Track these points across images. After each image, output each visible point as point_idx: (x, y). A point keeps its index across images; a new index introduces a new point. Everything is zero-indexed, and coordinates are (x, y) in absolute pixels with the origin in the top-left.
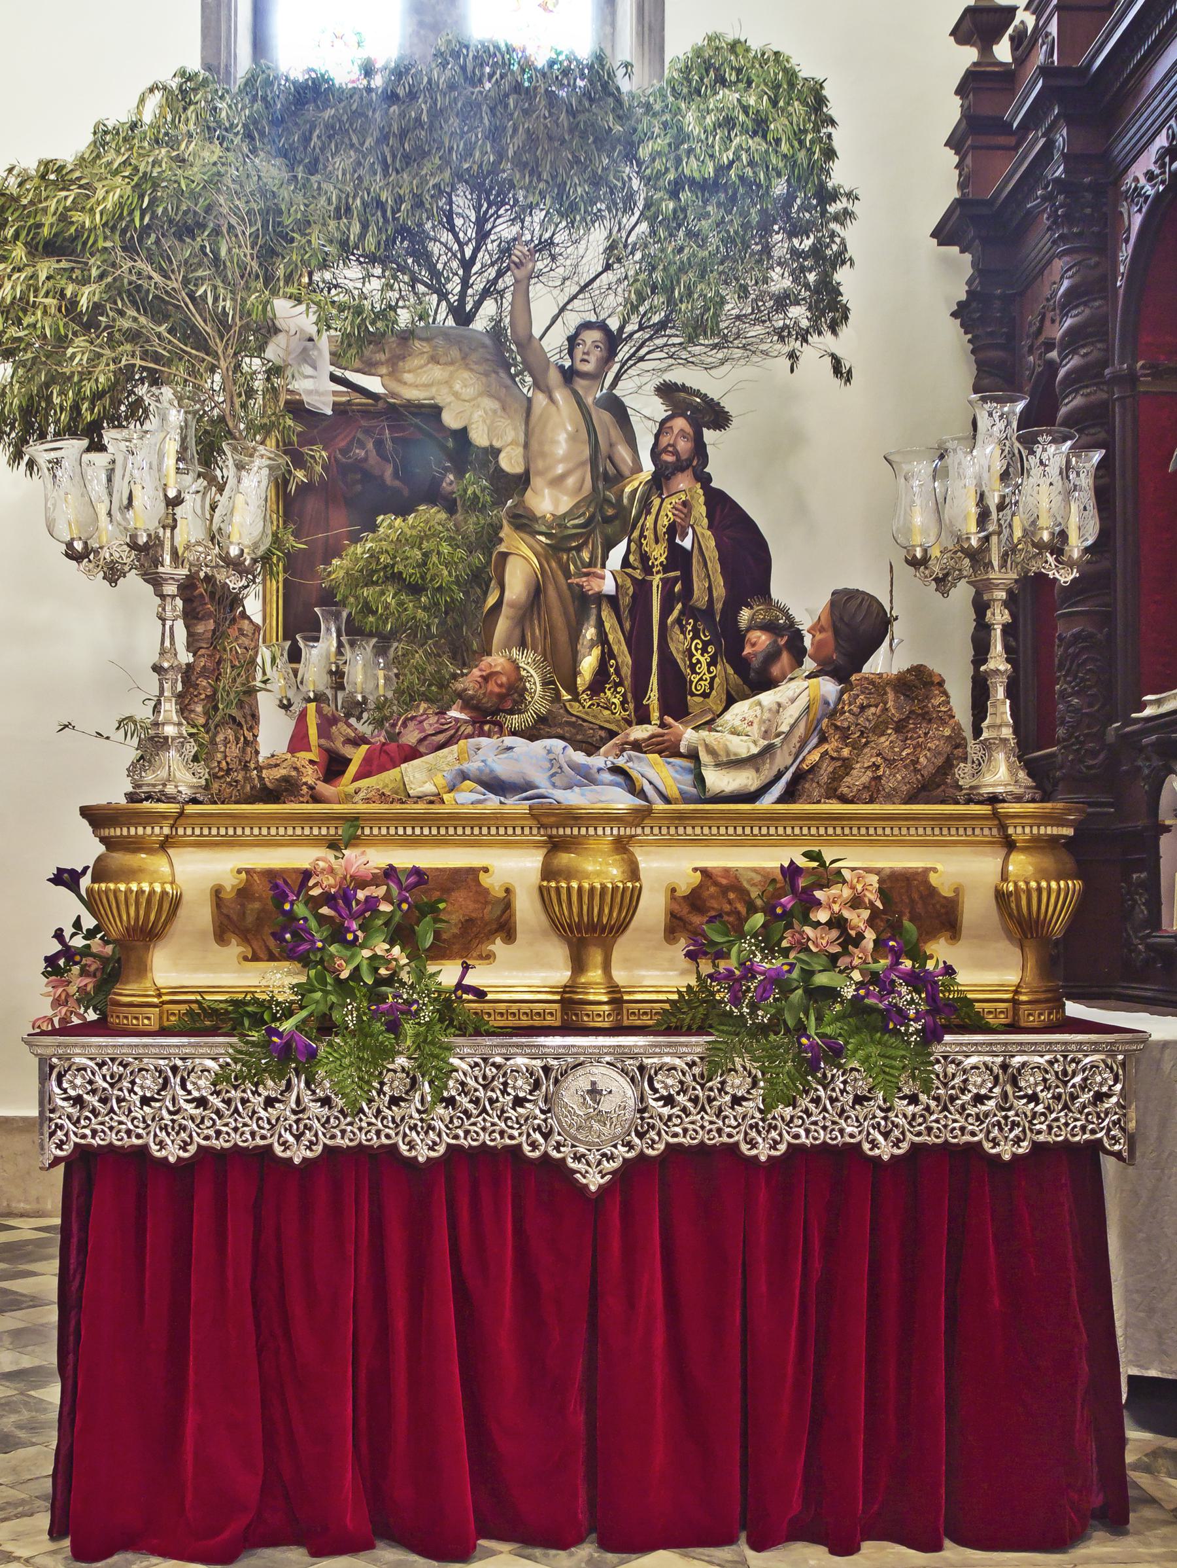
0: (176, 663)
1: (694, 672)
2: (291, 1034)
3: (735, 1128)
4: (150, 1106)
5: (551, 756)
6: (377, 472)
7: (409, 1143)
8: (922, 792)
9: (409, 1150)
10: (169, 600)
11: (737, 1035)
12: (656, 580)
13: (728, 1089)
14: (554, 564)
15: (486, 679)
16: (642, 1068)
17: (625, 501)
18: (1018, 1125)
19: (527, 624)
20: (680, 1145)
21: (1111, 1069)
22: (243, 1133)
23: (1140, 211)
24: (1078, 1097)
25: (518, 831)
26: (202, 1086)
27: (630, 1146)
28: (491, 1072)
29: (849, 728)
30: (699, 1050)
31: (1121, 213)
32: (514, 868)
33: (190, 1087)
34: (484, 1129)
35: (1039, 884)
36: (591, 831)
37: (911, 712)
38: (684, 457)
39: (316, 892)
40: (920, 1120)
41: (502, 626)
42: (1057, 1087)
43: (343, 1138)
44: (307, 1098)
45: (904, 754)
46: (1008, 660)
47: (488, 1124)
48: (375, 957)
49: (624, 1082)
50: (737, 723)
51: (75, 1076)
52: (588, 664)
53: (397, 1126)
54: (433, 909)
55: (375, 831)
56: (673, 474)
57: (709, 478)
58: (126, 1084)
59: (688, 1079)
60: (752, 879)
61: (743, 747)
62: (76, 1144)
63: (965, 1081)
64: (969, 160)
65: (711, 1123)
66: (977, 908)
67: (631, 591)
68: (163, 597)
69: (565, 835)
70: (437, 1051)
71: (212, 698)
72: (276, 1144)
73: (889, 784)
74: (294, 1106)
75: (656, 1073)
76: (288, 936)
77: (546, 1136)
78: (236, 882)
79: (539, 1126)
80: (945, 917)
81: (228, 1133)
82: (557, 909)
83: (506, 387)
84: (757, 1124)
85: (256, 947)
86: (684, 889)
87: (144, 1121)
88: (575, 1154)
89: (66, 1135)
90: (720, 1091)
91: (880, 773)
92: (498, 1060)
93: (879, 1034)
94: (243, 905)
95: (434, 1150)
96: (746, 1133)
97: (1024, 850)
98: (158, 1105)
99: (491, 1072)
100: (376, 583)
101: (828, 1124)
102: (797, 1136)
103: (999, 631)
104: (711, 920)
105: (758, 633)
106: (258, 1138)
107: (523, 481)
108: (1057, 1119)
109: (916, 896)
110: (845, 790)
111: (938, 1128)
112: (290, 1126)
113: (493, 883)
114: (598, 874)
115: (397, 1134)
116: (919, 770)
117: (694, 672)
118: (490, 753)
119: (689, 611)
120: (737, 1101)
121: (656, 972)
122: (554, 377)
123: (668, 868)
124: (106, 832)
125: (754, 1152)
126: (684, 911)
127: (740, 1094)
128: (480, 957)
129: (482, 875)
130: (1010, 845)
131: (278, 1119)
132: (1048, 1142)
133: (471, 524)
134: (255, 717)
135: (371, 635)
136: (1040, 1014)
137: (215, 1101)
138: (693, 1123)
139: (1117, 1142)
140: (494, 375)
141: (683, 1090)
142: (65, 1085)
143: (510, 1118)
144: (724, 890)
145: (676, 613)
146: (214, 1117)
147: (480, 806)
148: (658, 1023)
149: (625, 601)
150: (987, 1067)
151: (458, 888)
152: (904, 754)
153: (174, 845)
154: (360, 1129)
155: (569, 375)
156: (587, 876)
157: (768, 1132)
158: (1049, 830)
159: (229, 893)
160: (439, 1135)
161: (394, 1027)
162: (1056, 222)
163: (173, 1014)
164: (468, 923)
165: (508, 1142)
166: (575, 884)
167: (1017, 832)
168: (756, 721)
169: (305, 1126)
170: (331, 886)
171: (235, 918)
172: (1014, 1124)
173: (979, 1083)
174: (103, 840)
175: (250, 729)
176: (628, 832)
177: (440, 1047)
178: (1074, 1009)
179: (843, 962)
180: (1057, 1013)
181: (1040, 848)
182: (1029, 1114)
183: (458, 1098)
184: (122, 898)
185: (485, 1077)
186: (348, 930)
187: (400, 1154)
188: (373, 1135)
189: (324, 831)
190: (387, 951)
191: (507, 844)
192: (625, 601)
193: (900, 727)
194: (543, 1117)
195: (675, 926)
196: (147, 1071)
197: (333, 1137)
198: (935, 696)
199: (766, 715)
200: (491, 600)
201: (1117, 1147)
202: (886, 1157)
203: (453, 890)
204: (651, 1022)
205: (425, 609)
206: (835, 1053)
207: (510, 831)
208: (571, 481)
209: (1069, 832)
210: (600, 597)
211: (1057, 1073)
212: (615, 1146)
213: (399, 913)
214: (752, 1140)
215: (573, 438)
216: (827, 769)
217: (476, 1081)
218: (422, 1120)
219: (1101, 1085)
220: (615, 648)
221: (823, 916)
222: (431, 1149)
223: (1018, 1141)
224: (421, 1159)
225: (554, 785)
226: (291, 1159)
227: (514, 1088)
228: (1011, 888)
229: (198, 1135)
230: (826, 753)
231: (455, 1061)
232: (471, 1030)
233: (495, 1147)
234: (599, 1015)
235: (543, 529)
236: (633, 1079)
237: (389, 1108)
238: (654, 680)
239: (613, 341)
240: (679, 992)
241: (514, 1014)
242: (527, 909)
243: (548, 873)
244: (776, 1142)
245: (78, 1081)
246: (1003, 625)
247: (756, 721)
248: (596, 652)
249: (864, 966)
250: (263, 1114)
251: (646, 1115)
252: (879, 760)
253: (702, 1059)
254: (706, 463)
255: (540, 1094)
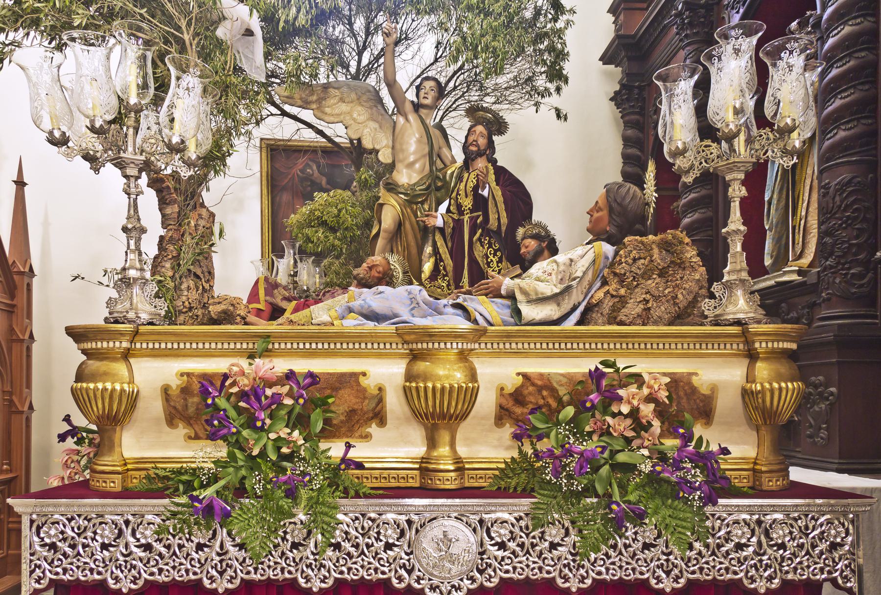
0: (138, 225)
1: (489, 266)
2: (211, 500)
3: (552, 566)
4: (108, 550)
5: (411, 296)
6: (318, 181)
7: (306, 578)
8: (678, 318)
9: (306, 583)
10: (132, 180)
11: (555, 498)
12: (466, 218)
13: (547, 538)
14: (409, 210)
15: (370, 268)
16: (481, 522)
17: (448, 178)
18: (771, 567)
19: (394, 244)
20: (511, 579)
21: (843, 525)
22: (179, 570)
23: (738, 12)
24: (817, 546)
25: (388, 346)
26: (147, 535)
27: (472, 579)
28: (367, 524)
29: (625, 274)
30: (526, 508)
31: (724, 18)
32: (385, 373)
33: (138, 536)
34: (362, 567)
35: (780, 385)
36: (442, 345)
37: (672, 262)
38: (482, 148)
39: (235, 390)
40: (695, 562)
41: (380, 243)
42: (801, 538)
43: (255, 573)
44: (228, 545)
45: (666, 292)
46: (744, 224)
47: (366, 563)
48: (279, 438)
49: (468, 532)
50: (540, 274)
51: (50, 528)
52: (428, 267)
53: (297, 564)
54: (323, 404)
55: (283, 346)
56: (476, 158)
57: (496, 161)
58: (90, 534)
59: (517, 530)
60: (560, 381)
61: (549, 289)
62: (50, 579)
63: (729, 533)
64: (622, 17)
65: (534, 562)
66: (728, 402)
67: (452, 225)
68: (126, 177)
69: (422, 349)
70: (326, 510)
71: (177, 258)
72: (205, 579)
73: (656, 313)
74: (218, 550)
75: (492, 525)
76: (216, 422)
77: (410, 572)
78: (179, 382)
79: (404, 564)
80: (705, 410)
81: (168, 570)
82: (416, 403)
83: (382, 115)
84: (569, 564)
85: (197, 430)
86: (510, 388)
87: (104, 562)
88: (431, 585)
89: (43, 572)
90: (540, 538)
91: (650, 305)
92: (373, 515)
93: (670, 501)
94: (185, 399)
95: (325, 583)
96: (561, 571)
97: (765, 359)
98: (114, 549)
99: (367, 524)
100: (313, 227)
101: (624, 564)
102: (599, 573)
103: (737, 203)
104: (532, 412)
105: (529, 240)
106: (191, 574)
107: (392, 167)
108: (801, 563)
109: (682, 393)
110: (624, 318)
111: (708, 569)
112: (216, 564)
113: (369, 383)
114: (447, 377)
115: (297, 571)
116: (677, 304)
117: (489, 266)
118: (370, 298)
119: (487, 232)
120: (553, 546)
121: (486, 446)
122: (408, 107)
123: (498, 373)
124: (88, 345)
125: (567, 585)
126: (510, 404)
127: (556, 541)
128: (361, 437)
129: (361, 378)
130: (752, 356)
131: (206, 560)
132: (794, 580)
133: (364, 196)
134: (211, 273)
135: (311, 255)
136: (777, 480)
137: (159, 547)
138: (520, 562)
139: (849, 580)
140: (375, 109)
141: (513, 539)
142: (42, 535)
143: (382, 559)
144: (540, 389)
145: (478, 235)
146: (157, 558)
147: (359, 328)
148: (491, 485)
149: (448, 231)
150: (746, 523)
151: (344, 387)
152: (666, 292)
153: (134, 356)
154: (269, 567)
155: (417, 107)
156: (439, 378)
157: (578, 570)
158: (781, 345)
159: (174, 391)
160: (329, 571)
161: (291, 494)
162: (682, 28)
163: (136, 478)
164: (352, 412)
165: (381, 576)
166: (430, 385)
167: (760, 346)
168: (554, 273)
169: (227, 565)
170: (245, 385)
171: (180, 408)
172: (768, 566)
173: (739, 534)
174: (84, 352)
175: (208, 281)
176: (469, 347)
177: (328, 507)
178: (797, 474)
179: (635, 443)
180: (783, 480)
181: (774, 358)
182: (779, 559)
183: (342, 543)
184: (91, 395)
185: (363, 528)
186: (257, 419)
187: (300, 586)
188: (278, 571)
189: (245, 346)
190: (289, 434)
191: (380, 355)
192: (448, 231)
193: (662, 273)
194: (407, 558)
195: (502, 415)
196: (106, 524)
197: (248, 573)
198: (687, 251)
199: (562, 268)
200: (374, 232)
201: (849, 585)
202: (668, 590)
203: (340, 389)
204: (485, 484)
205: (339, 240)
206: (639, 517)
207: (382, 346)
208: (417, 166)
209: (794, 346)
210: (435, 228)
211: (800, 527)
212: (462, 580)
213: (298, 407)
214: (565, 575)
215: (419, 141)
216: (608, 304)
217: (357, 531)
218: (315, 560)
219: (835, 537)
220: (443, 256)
221: (625, 409)
222: (323, 581)
223: (770, 579)
224: (315, 590)
225: (413, 316)
226: (216, 590)
227: (385, 536)
228: (759, 387)
229: (145, 572)
230: (608, 292)
231: (340, 517)
232: (352, 493)
233: (371, 580)
234: (448, 480)
235: (403, 191)
236: (474, 530)
237: (291, 551)
238: (466, 272)
239: (441, 91)
240: (505, 462)
241: (385, 478)
242: (394, 403)
243: (410, 376)
244: (583, 578)
245: (53, 532)
246: (741, 198)
247: (554, 273)
248: (432, 260)
249: (654, 447)
250: (195, 555)
251: (485, 556)
252: (648, 297)
253: (527, 515)
254: (494, 152)
255: (404, 542)
